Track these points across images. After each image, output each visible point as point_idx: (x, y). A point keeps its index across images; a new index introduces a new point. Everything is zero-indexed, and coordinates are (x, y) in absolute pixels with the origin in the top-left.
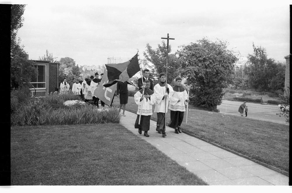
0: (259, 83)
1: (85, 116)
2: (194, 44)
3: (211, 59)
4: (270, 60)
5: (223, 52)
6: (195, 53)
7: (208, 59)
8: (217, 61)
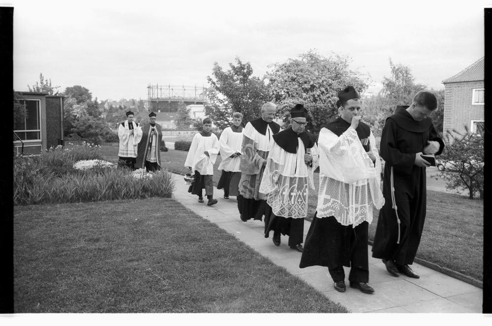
1: (111, 187)
6: (295, 76)
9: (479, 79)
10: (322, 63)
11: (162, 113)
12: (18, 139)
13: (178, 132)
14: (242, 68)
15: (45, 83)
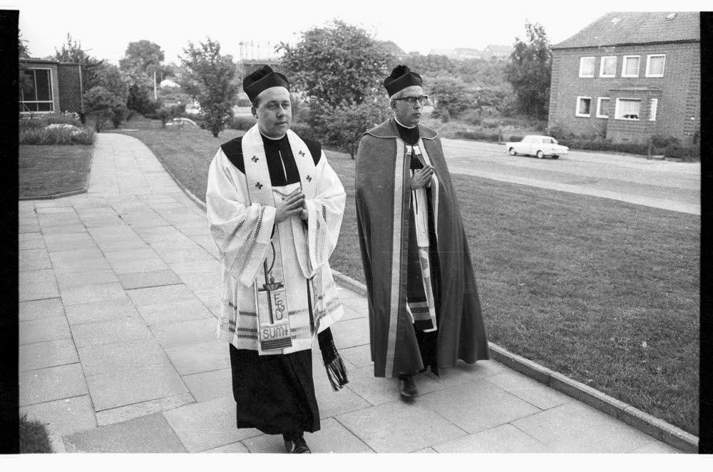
1: (50, 137)
9: (679, 38)
12: (26, 110)
15: (73, 45)
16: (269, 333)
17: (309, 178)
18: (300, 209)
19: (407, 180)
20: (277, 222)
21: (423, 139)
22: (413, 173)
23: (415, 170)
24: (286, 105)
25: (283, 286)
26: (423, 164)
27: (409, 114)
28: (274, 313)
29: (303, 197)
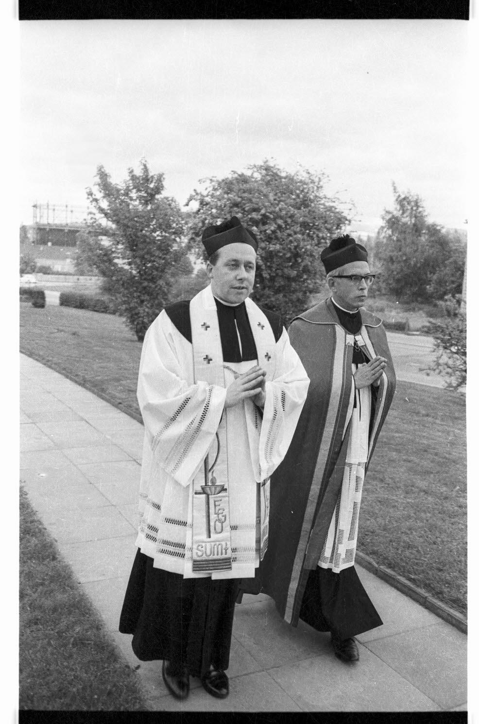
0: (406, 284)
2: (239, 175)
3: (281, 218)
4: (434, 225)
5: (312, 201)
6: (239, 199)
7: (272, 216)
8: (297, 223)
10: (283, 180)
11: (54, 247)
13: (76, 277)
14: (147, 179)
16: (203, 549)
17: (268, 357)
18: (259, 390)
19: (348, 376)
20: (227, 408)
21: (366, 326)
22: (357, 367)
23: (359, 365)
24: (250, 267)
25: (226, 489)
26: (370, 358)
27: (352, 296)
28: (212, 524)
29: (264, 375)
